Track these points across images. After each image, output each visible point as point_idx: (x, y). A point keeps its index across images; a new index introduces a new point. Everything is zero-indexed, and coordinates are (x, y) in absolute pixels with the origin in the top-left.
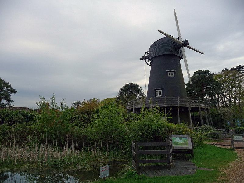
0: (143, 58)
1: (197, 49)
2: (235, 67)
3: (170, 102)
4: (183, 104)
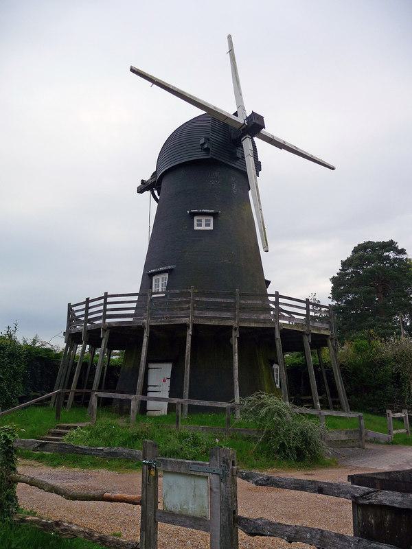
0: (144, 187)
1: (166, 81)
3: (163, 310)
4: (208, 314)
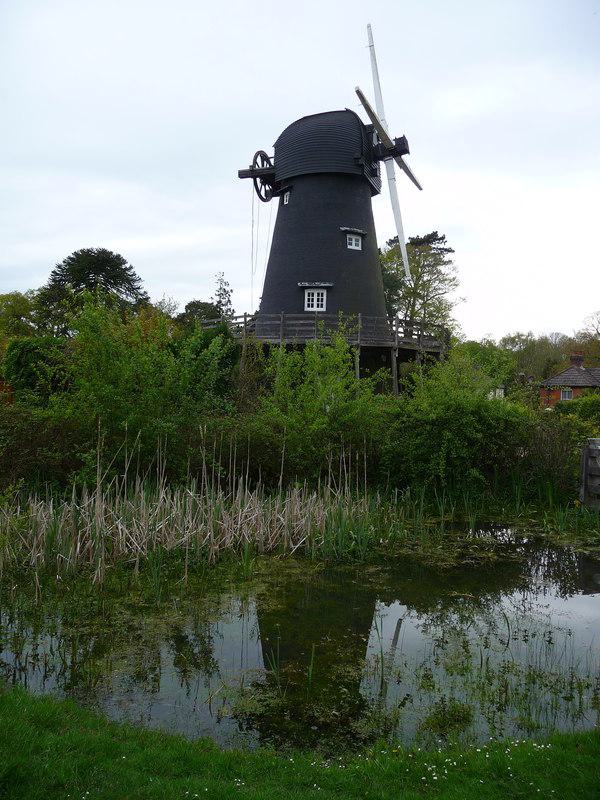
2: (422, 236)
